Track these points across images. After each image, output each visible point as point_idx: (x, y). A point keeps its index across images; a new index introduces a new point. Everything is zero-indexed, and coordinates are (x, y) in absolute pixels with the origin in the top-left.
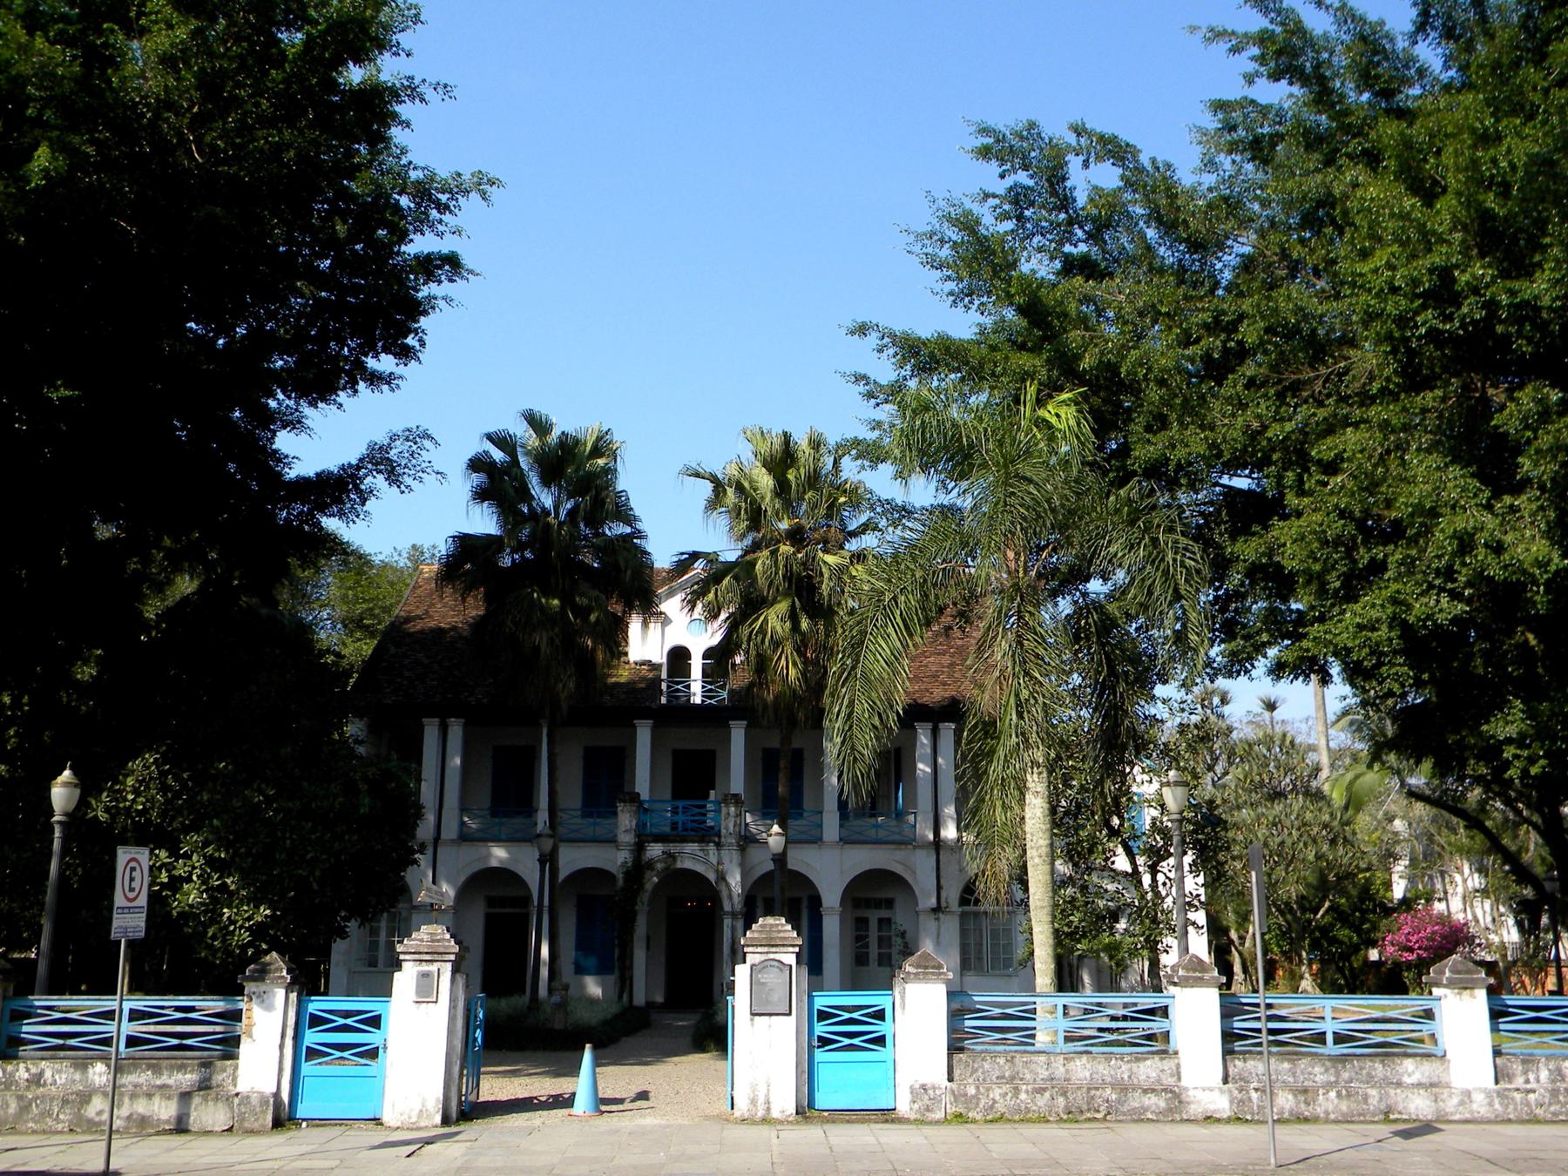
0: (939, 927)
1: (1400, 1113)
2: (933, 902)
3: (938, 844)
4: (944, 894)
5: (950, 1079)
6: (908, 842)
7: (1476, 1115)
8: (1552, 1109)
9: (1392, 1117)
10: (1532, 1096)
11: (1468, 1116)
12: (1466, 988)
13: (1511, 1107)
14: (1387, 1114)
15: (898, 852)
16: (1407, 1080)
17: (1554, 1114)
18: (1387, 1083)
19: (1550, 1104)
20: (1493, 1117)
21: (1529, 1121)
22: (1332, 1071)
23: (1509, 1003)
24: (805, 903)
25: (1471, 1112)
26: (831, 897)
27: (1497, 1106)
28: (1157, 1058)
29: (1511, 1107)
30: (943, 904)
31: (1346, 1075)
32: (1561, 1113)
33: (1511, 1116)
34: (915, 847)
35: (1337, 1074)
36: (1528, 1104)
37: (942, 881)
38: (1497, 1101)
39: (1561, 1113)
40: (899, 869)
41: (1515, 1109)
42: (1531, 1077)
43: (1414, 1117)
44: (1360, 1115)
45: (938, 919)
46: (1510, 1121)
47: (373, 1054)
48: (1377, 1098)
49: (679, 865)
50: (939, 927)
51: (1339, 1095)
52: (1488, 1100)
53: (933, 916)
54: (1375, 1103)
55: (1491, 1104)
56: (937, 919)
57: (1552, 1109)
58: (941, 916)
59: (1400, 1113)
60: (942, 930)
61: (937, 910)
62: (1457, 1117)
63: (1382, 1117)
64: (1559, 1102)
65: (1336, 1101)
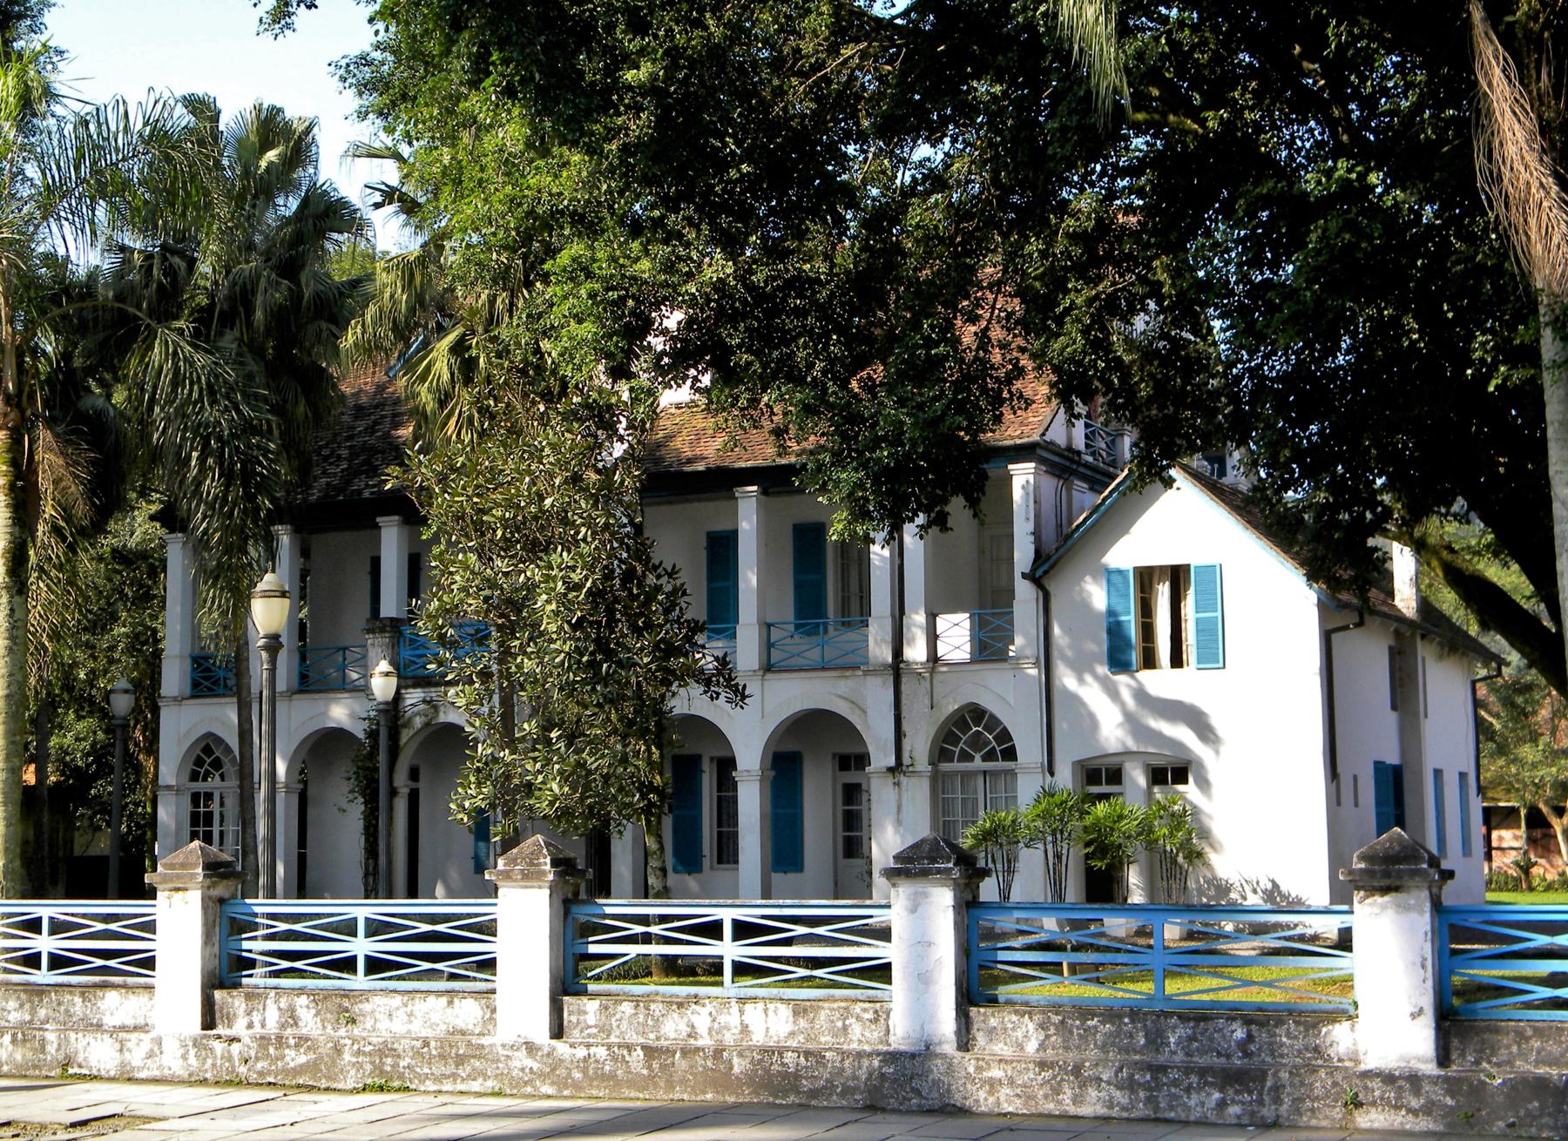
0: (900, 795)
1: (80, 1066)
2: (892, 761)
3: (898, 666)
4: (907, 745)
5: (558, 1031)
6: (853, 664)
7: (166, 1072)
8: (259, 1065)
9: (71, 1071)
10: (236, 1047)
11: (156, 1073)
12: (178, 889)
13: (209, 1061)
14: (65, 1066)
15: (842, 683)
16: (109, 1021)
17: (261, 1074)
18: (68, 1025)
19: (257, 1059)
20: (186, 1075)
21: (229, 1083)
22: (27, 1006)
23: (608, 910)
24: (706, 766)
25: (160, 1067)
26: (749, 757)
27: (192, 1060)
28: (444, 1000)
29: (209, 1061)
30: (906, 760)
31: (42, 1013)
32: (269, 1073)
33: (208, 1075)
34: (866, 673)
35: (33, 1012)
36: (230, 1059)
37: (906, 726)
38: (192, 1052)
39: (269, 1073)
40: (842, 708)
41: (214, 1065)
42: (256, 1018)
43: (95, 1072)
44: (35, 1067)
45: (897, 784)
46: (203, 1082)
47: (493, 992)
48: (55, 1045)
49: (442, 718)
50: (900, 795)
51: (14, 1041)
52: (182, 1051)
53: (890, 780)
54: (53, 1051)
55: (184, 1057)
56: (897, 784)
57: (259, 1065)
58: (903, 780)
59: (80, 1066)
60: (905, 797)
61: (897, 769)
62: (143, 1075)
63: (59, 1071)
64: (269, 1055)
65: (10, 1048)
